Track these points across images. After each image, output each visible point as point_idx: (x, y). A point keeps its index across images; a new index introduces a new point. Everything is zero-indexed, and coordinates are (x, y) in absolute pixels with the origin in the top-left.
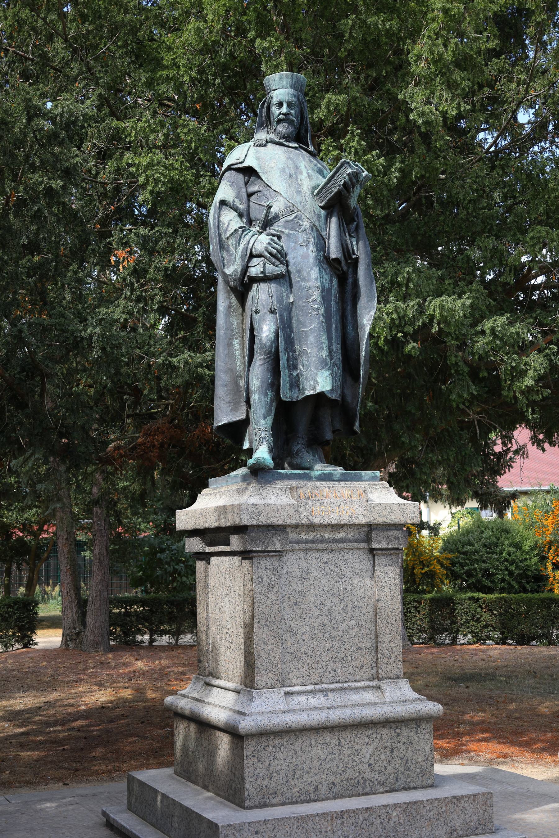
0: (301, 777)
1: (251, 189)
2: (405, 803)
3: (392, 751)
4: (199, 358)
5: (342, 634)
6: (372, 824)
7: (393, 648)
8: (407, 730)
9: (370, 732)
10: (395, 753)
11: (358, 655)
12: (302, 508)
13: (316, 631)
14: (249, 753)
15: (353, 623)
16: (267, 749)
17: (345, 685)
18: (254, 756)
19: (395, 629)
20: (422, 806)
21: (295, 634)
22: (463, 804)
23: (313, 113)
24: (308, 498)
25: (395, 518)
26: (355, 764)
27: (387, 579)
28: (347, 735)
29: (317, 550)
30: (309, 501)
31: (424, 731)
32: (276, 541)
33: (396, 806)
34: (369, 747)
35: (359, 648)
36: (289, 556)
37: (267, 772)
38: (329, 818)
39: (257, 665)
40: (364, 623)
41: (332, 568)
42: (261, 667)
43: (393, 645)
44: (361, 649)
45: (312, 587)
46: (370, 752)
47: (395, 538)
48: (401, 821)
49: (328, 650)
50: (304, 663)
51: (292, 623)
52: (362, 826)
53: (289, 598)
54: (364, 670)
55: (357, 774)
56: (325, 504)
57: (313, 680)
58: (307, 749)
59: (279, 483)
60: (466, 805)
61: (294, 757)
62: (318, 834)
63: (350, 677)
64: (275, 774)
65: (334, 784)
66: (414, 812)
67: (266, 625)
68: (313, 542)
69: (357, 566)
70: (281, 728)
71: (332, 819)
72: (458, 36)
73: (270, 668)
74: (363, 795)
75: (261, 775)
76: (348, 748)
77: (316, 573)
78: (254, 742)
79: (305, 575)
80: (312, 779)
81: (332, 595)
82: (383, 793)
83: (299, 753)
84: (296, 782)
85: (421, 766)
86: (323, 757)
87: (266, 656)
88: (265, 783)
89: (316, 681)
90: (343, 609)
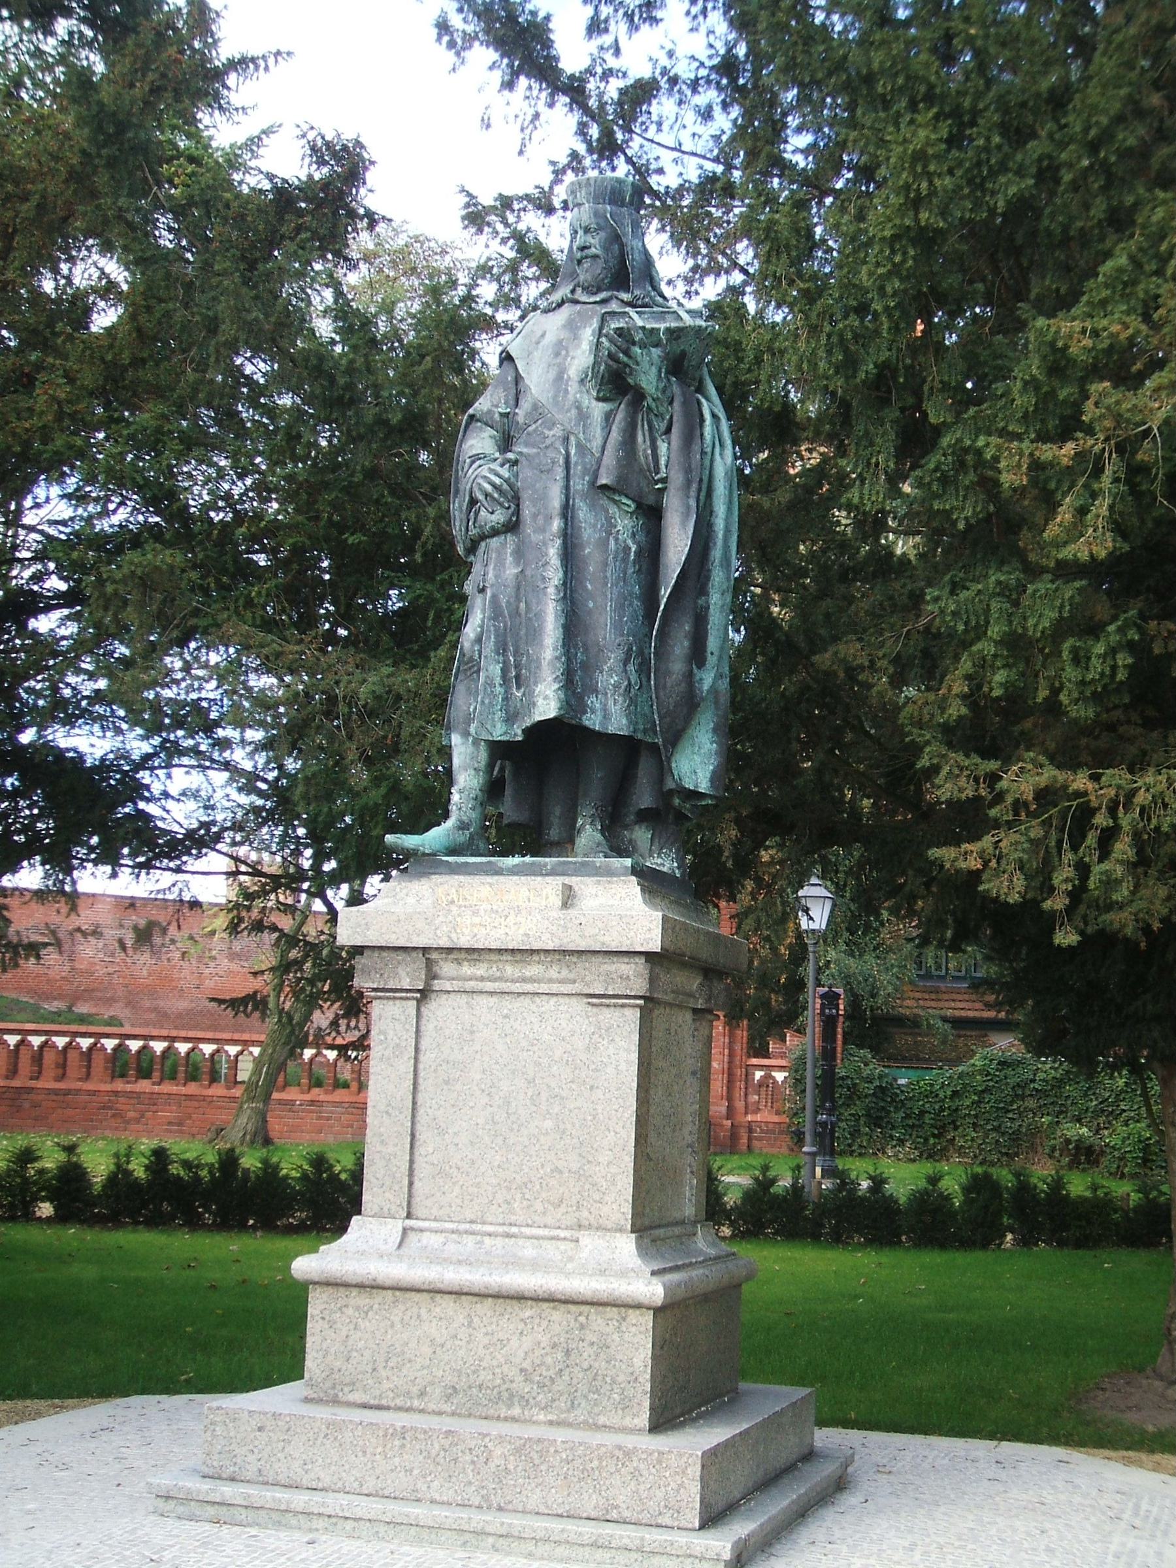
0: (399, 1367)
3: (568, 1353)
4: (406, 679)
9: (528, 1313)
10: (573, 1357)
11: (553, 1182)
12: (441, 919)
13: (480, 1132)
15: (548, 1124)
17: (514, 1230)
20: (552, 1450)
21: (442, 1132)
24: (452, 902)
26: (495, 1363)
27: (611, 1051)
29: (492, 993)
30: (454, 908)
31: (633, 1329)
33: (501, 1439)
35: (557, 1170)
40: (569, 1126)
41: (516, 1025)
42: (373, 1180)
43: (613, 1169)
44: (561, 1172)
45: (478, 1056)
48: (511, 1467)
54: (563, 1209)
55: (498, 1381)
56: (482, 913)
58: (412, 1322)
60: (642, 1466)
63: (536, 1218)
64: (354, 1354)
66: (535, 1456)
68: (482, 979)
71: (385, 1436)
72: (42, 52)
73: (388, 1183)
74: (506, 1419)
75: (332, 1350)
76: (487, 1334)
78: (325, 1296)
80: (418, 1374)
84: (390, 1373)
86: (439, 1341)
88: (338, 1364)
89: (473, 1217)
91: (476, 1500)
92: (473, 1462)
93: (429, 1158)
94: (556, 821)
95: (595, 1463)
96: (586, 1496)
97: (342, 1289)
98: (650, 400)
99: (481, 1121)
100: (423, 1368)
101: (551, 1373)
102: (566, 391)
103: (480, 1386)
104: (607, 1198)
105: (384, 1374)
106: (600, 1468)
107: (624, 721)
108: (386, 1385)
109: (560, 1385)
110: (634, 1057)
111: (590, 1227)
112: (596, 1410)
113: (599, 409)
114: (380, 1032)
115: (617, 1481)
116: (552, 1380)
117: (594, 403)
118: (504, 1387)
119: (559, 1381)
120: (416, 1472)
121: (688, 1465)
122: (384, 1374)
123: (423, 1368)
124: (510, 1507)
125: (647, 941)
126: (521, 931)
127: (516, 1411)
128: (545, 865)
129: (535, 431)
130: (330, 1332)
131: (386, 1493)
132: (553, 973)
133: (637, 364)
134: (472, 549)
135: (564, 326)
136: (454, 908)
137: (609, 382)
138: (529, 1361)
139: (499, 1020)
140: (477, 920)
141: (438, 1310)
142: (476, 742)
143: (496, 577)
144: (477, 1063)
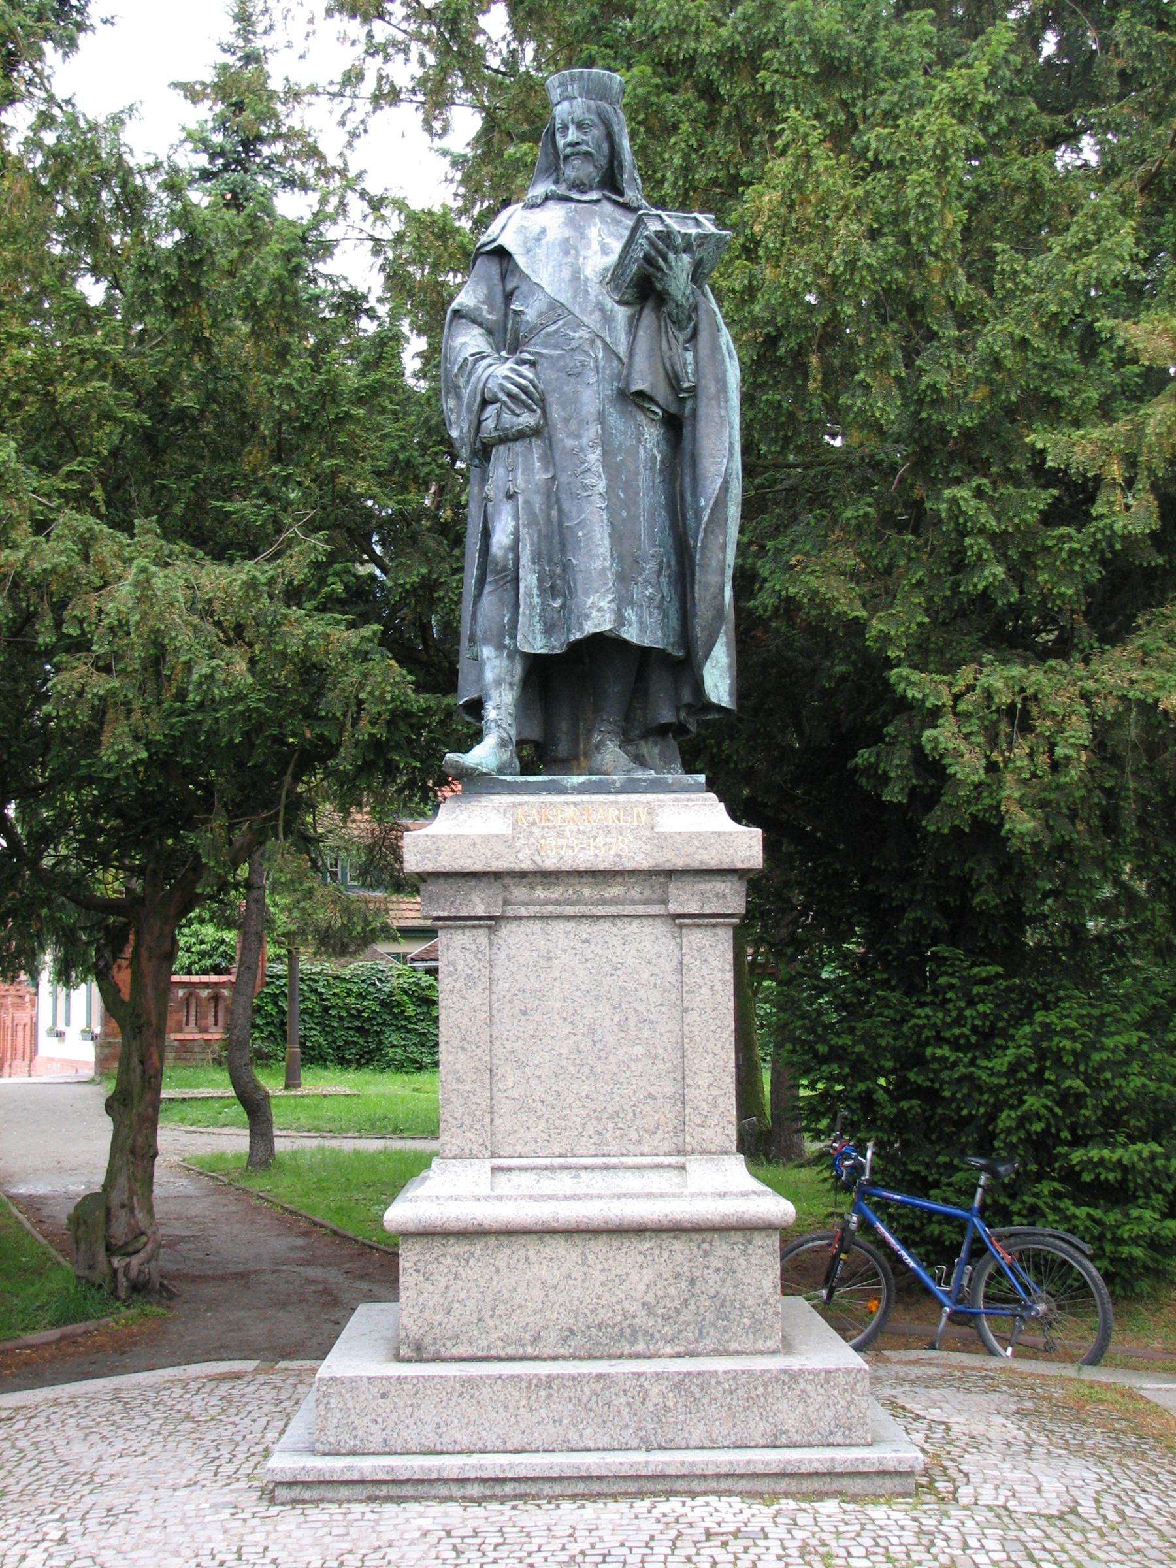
1: (510, 287)
2: (679, 1373)
3: (692, 1281)
5: (616, 1070)
6: (609, 1404)
7: (715, 1098)
8: (724, 1246)
9: (647, 1245)
11: (647, 1109)
12: (522, 841)
13: (564, 1063)
14: (407, 1265)
15: (639, 1050)
16: (442, 1259)
18: (418, 1271)
19: (721, 1063)
20: (713, 1381)
21: (521, 1065)
22: (802, 1386)
23: (377, 107)
24: (534, 824)
25: (711, 859)
26: (614, 1299)
27: (705, 971)
28: (598, 1246)
29: (568, 918)
30: (536, 830)
31: (760, 1251)
32: (477, 900)
34: (644, 1271)
36: (513, 926)
37: (442, 1301)
38: (524, 1385)
39: (443, 1117)
40: (661, 1051)
41: (597, 950)
42: (450, 1120)
43: (715, 1092)
44: (655, 1098)
45: (557, 984)
46: (646, 1280)
47: (717, 895)
48: (670, 1404)
49: (587, 1096)
50: (539, 1118)
51: (516, 1045)
52: (589, 1406)
53: (511, 1001)
56: (568, 834)
57: (558, 1150)
59: (496, 799)
60: (809, 1388)
61: (495, 1278)
62: (501, 1410)
63: (631, 1147)
64: (456, 1305)
65: (571, 1331)
67: (462, 1048)
68: (557, 903)
69: (649, 947)
70: (463, 1225)
71: (529, 1387)
73: (468, 1122)
75: (430, 1304)
76: (603, 1270)
77: (565, 959)
79: (543, 963)
81: (597, 999)
82: (671, 1357)
83: (504, 1271)
84: (498, 1322)
85: (753, 1313)
86: (551, 1282)
87: (462, 1101)
88: (438, 1318)
89: (562, 1151)
90: (618, 1024)
91: (635, 1443)
92: (628, 1404)
93: (510, 1093)
94: (563, 737)
95: (761, 1390)
96: (752, 1424)
97: (438, 1241)
98: (672, 305)
99: (564, 1051)
100: (535, 1312)
101: (677, 1303)
102: (587, 293)
103: (600, 1326)
104: (709, 1121)
105: (491, 1323)
106: (765, 1395)
107: (659, 634)
108: (494, 1335)
109: (686, 1316)
110: (729, 976)
111: (693, 1152)
112: (726, 1337)
113: (621, 314)
114: (449, 964)
115: (784, 1405)
116: (678, 1311)
117: (617, 307)
118: (625, 1324)
119: (685, 1311)
120: (565, 1421)
121: (856, 1380)
122: (491, 1323)
123: (535, 1312)
124: (671, 1445)
125: (748, 858)
126: (612, 852)
127: (640, 1347)
128: (614, 783)
129: (557, 331)
130: (427, 1285)
131: (534, 1447)
132: (635, 894)
133: (670, 268)
134: (483, 452)
135: (565, 224)
136: (536, 830)
137: (636, 285)
138: (651, 1294)
139: (579, 945)
140: (563, 841)
141: (547, 1250)
142: (511, 656)
143: (527, 482)
144: (556, 991)
